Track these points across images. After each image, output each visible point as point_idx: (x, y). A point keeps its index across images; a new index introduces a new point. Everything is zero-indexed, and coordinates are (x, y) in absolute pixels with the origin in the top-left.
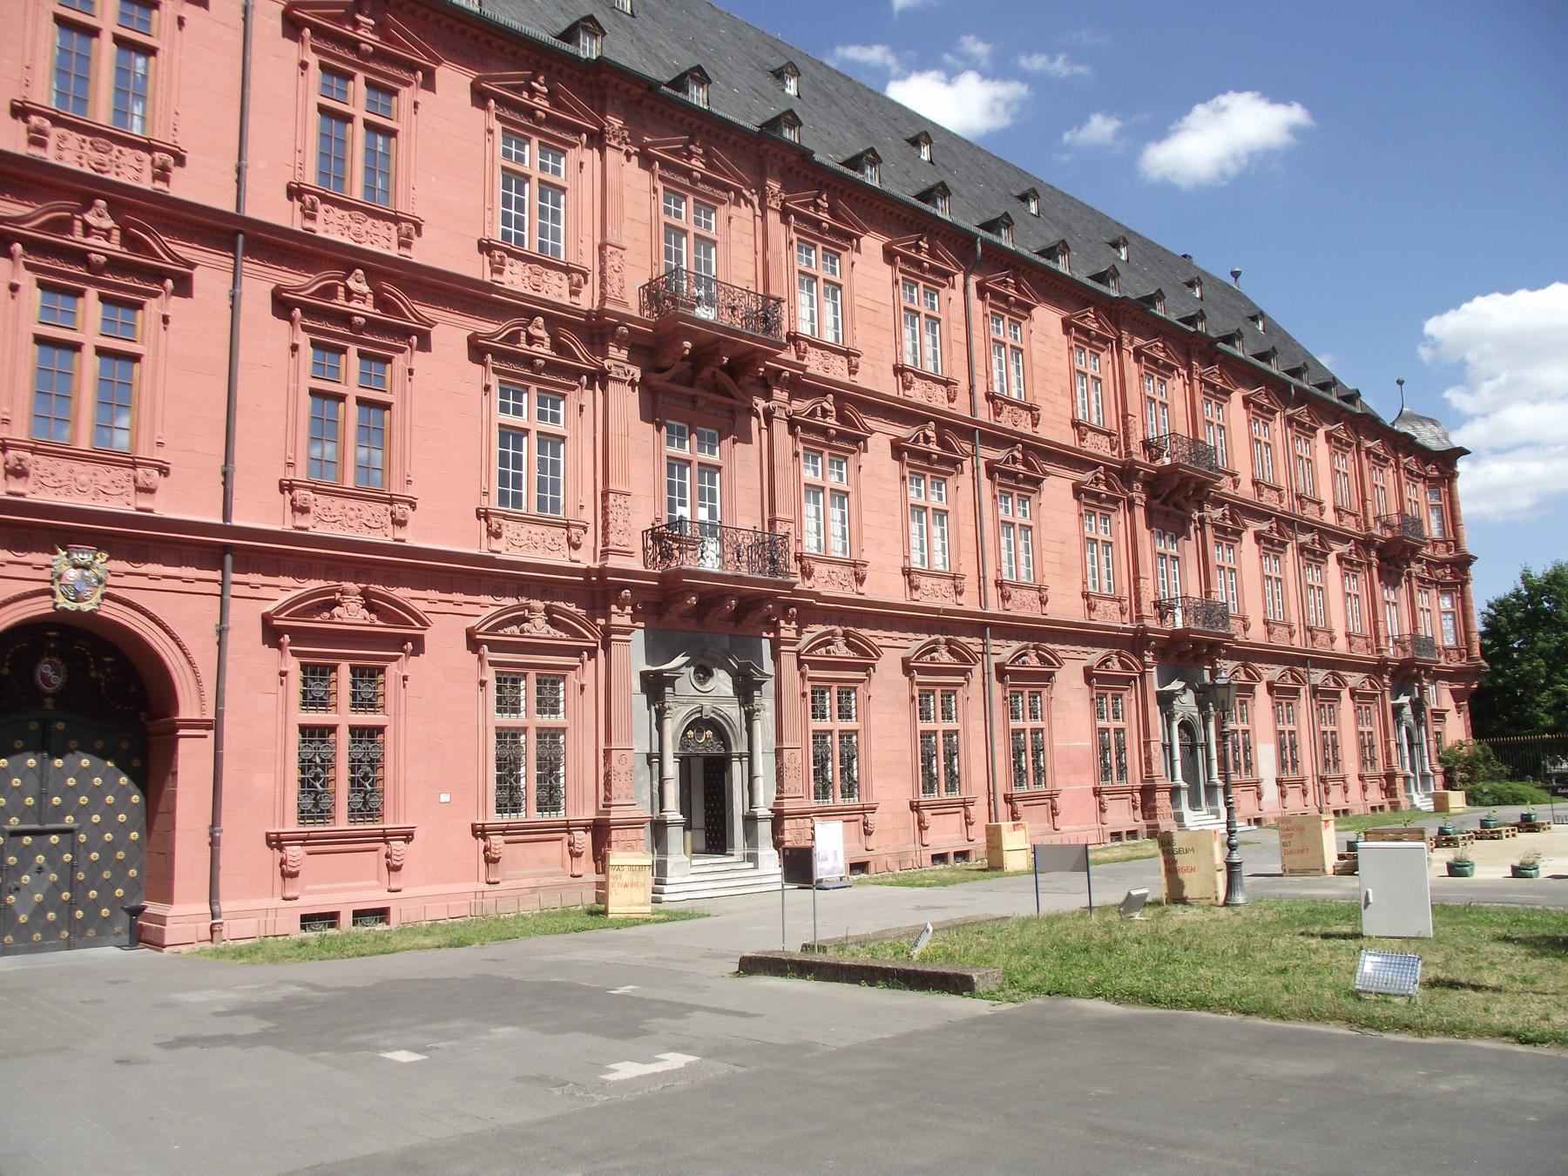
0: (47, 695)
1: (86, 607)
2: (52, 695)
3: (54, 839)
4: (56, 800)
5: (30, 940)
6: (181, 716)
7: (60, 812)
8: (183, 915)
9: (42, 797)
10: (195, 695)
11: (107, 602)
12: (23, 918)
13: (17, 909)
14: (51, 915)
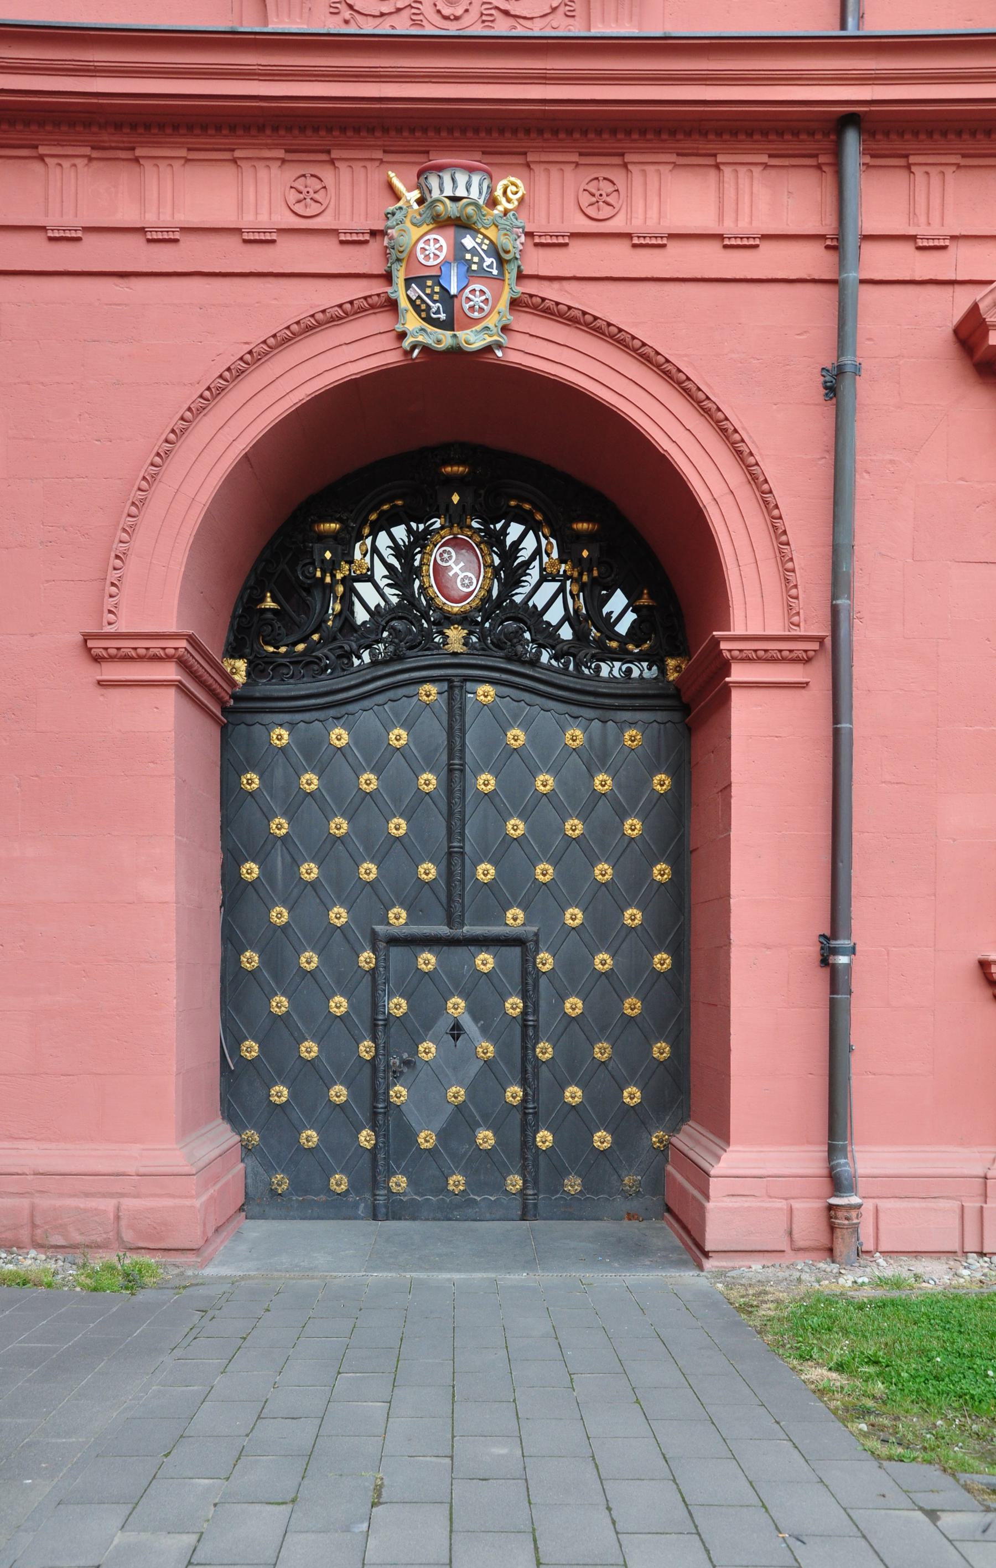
0: (448, 619)
1: (473, 339)
2: (464, 619)
3: (485, 961)
4: (485, 872)
5: (444, 1189)
6: (738, 628)
7: (496, 896)
8: (752, 1173)
9: (453, 862)
10: (769, 569)
11: (525, 322)
12: (426, 1139)
13: (413, 1117)
14: (486, 1138)
